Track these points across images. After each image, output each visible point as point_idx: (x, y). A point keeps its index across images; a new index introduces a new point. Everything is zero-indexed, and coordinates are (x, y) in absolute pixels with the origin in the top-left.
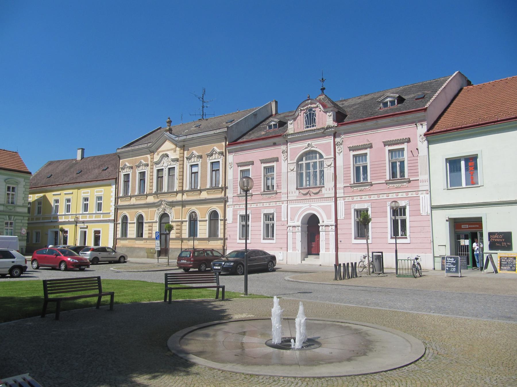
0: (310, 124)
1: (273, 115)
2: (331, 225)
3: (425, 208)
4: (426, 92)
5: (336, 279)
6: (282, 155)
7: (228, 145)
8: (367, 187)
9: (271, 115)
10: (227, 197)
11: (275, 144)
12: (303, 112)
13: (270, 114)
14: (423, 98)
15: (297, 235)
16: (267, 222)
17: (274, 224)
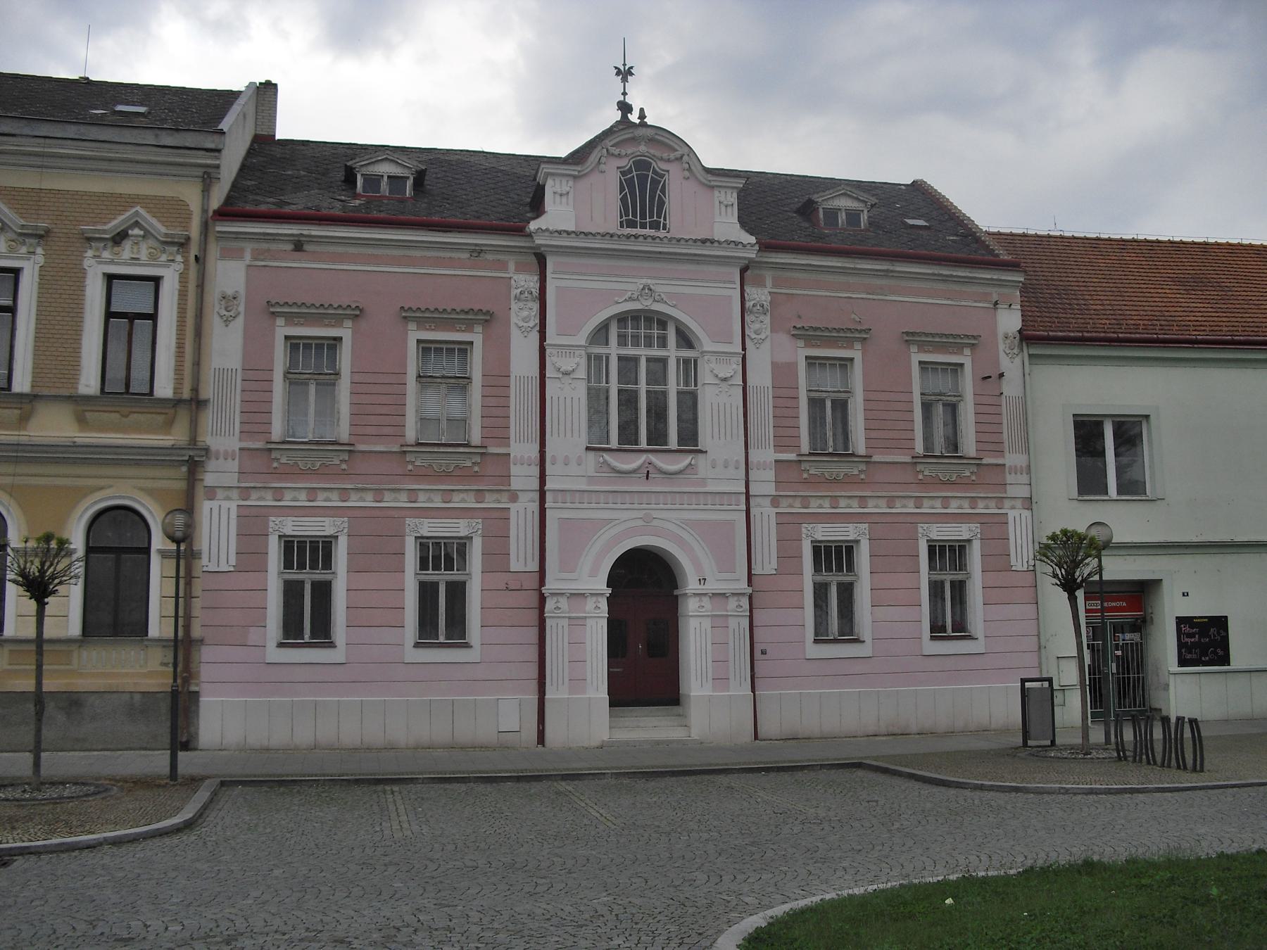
2: (734, 594)
15: (588, 628)
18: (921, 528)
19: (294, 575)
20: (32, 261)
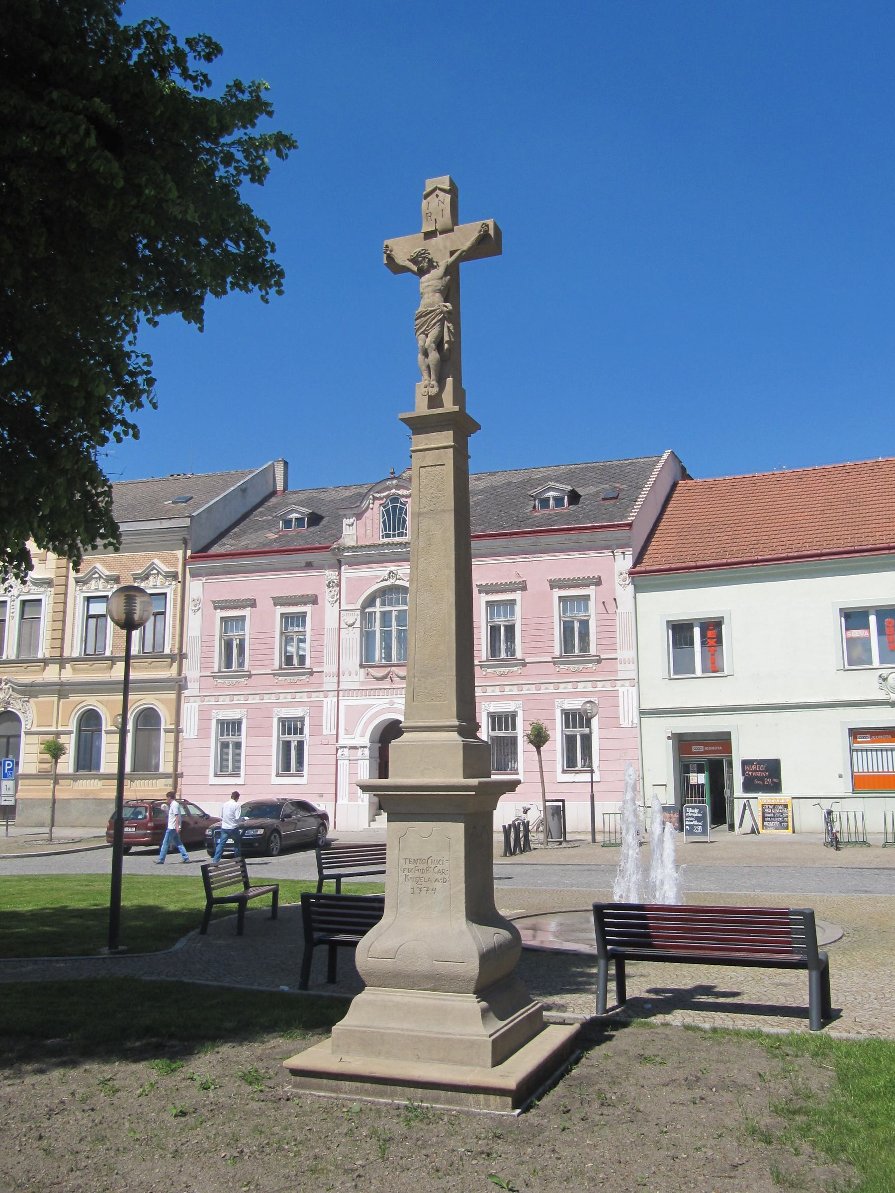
0: (394, 530)
1: (279, 493)
3: (628, 714)
4: (617, 485)
5: (505, 855)
6: (327, 590)
7: (191, 557)
8: (515, 669)
9: (274, 493)
10: (186, 678)
11: (309, 566)
12: (377, 503)
13: (271, 489)
14: (616, 498)
16: (287, 737)
17: (303, 741)
18: (276, 710)
19: (570, 731)
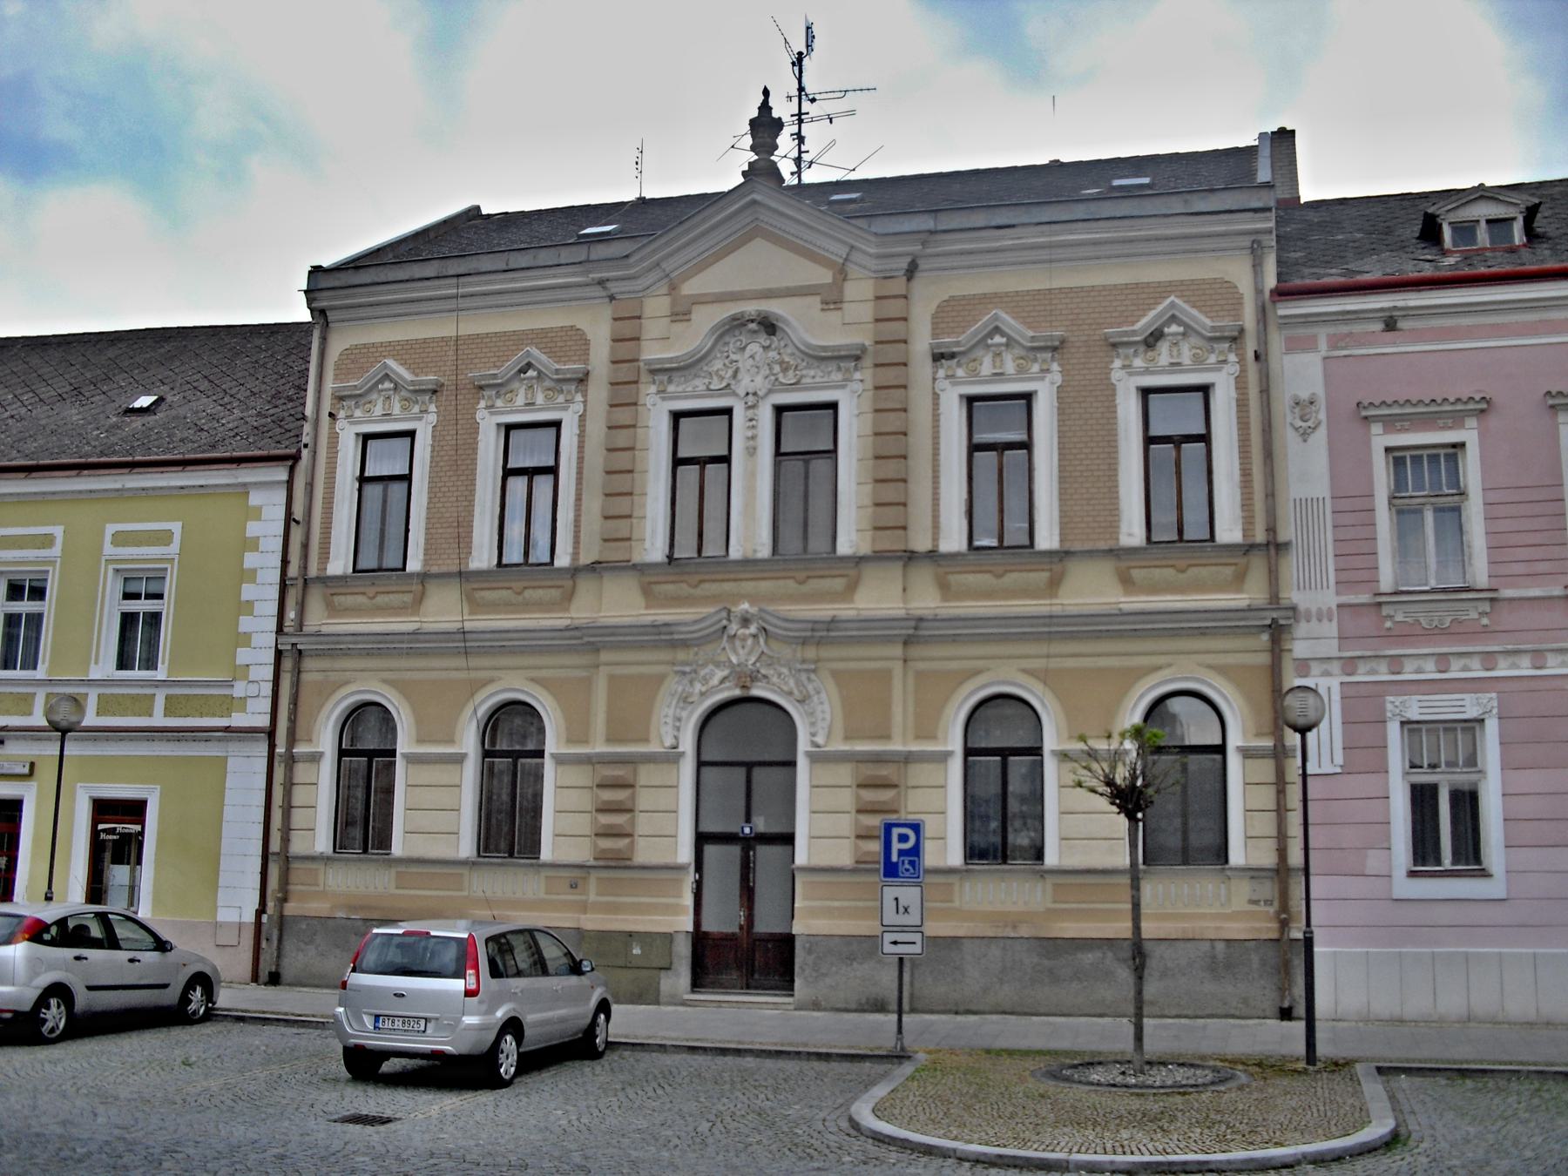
18: (1392, 703)
20: (424, 420)
